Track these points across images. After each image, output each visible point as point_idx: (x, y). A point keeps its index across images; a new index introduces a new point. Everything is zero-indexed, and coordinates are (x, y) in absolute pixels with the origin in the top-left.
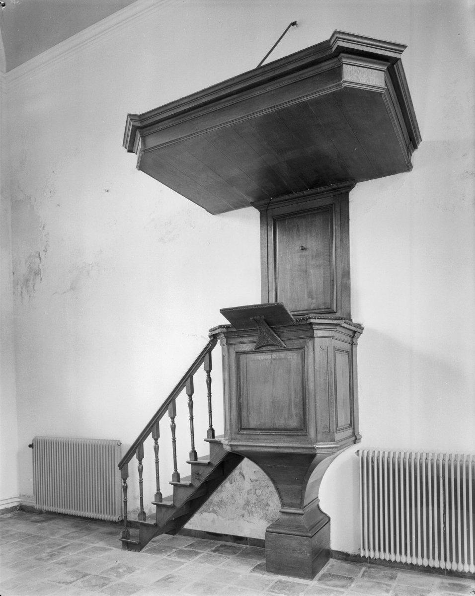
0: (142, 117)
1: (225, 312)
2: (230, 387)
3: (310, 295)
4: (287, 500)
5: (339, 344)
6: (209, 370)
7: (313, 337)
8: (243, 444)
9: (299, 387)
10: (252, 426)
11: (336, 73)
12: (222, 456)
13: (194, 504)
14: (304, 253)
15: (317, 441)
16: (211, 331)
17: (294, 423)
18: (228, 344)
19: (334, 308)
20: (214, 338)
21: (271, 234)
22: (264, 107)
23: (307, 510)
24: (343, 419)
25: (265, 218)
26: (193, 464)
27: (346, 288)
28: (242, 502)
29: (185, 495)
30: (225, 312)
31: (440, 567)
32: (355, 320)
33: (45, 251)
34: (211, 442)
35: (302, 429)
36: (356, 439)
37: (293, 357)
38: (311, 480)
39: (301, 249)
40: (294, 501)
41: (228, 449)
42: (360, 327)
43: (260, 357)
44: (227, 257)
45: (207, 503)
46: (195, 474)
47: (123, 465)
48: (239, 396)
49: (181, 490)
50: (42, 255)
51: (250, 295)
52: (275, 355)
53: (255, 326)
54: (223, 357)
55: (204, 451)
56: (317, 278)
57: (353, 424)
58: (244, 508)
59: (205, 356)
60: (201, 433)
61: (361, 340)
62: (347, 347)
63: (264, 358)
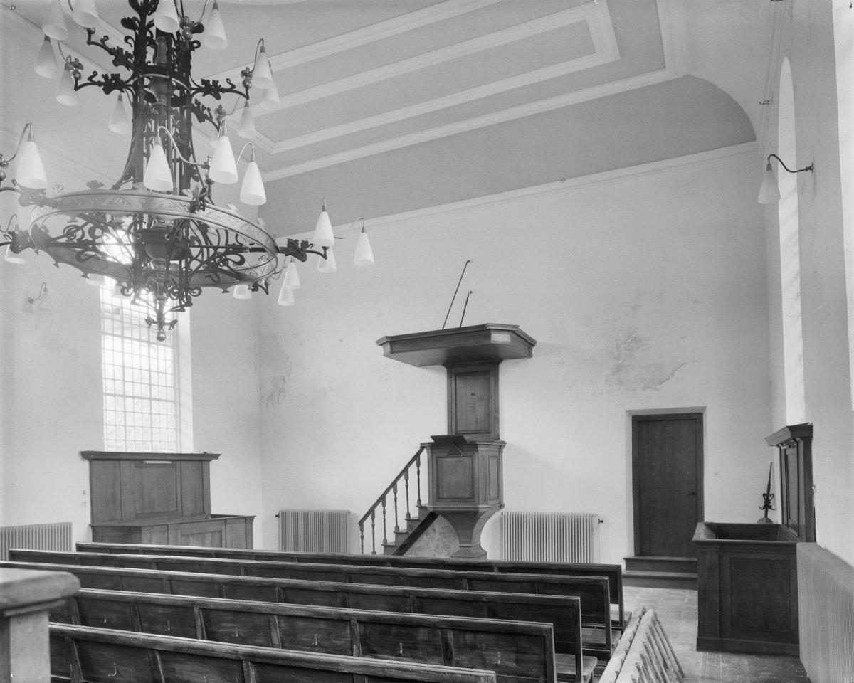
0: (392, 337)
1: (433, 437)
2: (433, 477)
3: (477, 422)
4: (462, 539)
5: (491, 453)
6: (418, 466)
7: (477, 451)
8: (441, 506)
9: (470, 477)
10: (445, 497)
11: (489, 336)
12: (426, 514)
13: (403, 548)
14: (473, 397)
15: (479, 504)
16: (421, 444)
17: (468, 495)
18: (432, 453)
19: (489, 429)
20: (422, 448)
21: (453, 383)
22: (456, 343)
23: (474, 545)
24: (493, 493)
25: (449, 373)
26: (408, 520)
27: (497, 420)
28: (434, 547)
29: (403, 539)
30: (433, 437)
31: (286, 255)
32: (502, 438)
33: (289, 375)
34: (419, 507)
35: (472, 498)
36: (501, 506)
37: (467, 461)
38: (476, 529)
39: (470, 389)
40: (467, 540)
41: (431, 510)
42: (504, 443)
43: (449, 460)
44: (425, 403)
45: (411, 548)
46: (409, 526)
47: (361, 523)
48: (438, 481)
49: (400, 536)
50: (287, 378)
51: (443, 431)
52: (458, 459)
53: (447, 447)
54: (428, 459)
55: (415, 514)
56: (480, 411)
57: (499, 496)
58: (435, 551)
59: (416, 458)
60: (413, 502)
61: (504, 450)
62: (497, 454)
63: (451, 460)
